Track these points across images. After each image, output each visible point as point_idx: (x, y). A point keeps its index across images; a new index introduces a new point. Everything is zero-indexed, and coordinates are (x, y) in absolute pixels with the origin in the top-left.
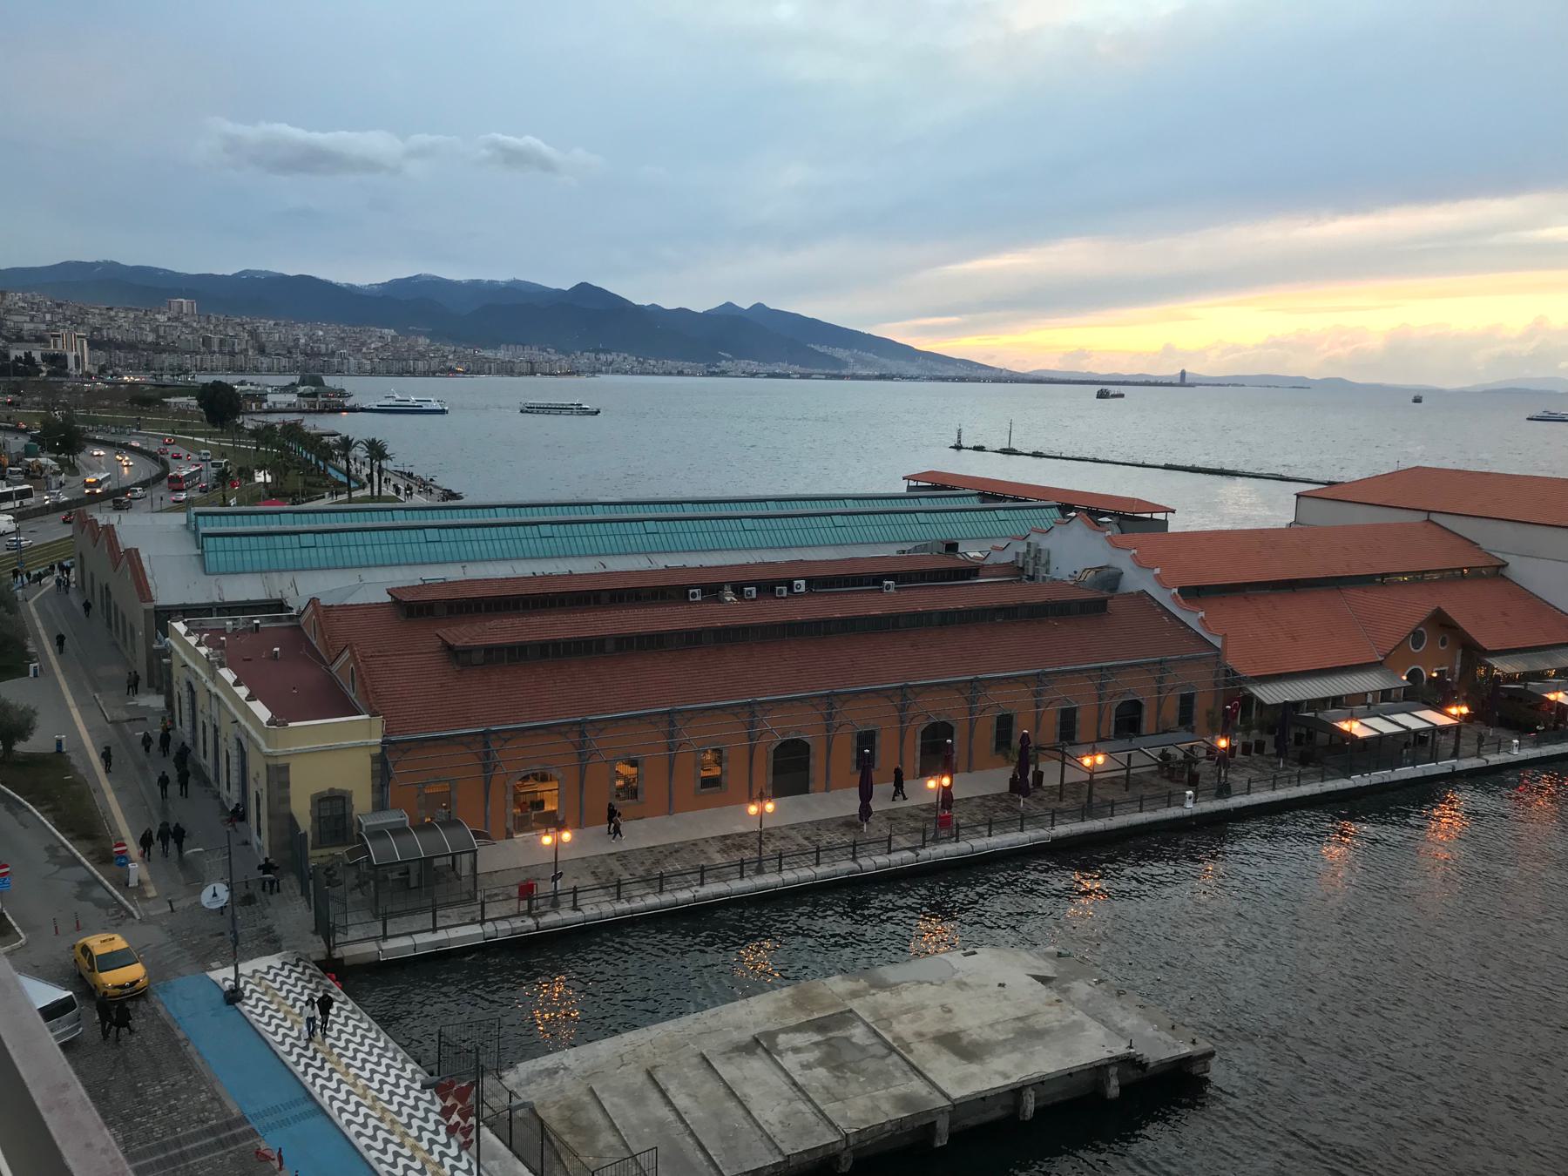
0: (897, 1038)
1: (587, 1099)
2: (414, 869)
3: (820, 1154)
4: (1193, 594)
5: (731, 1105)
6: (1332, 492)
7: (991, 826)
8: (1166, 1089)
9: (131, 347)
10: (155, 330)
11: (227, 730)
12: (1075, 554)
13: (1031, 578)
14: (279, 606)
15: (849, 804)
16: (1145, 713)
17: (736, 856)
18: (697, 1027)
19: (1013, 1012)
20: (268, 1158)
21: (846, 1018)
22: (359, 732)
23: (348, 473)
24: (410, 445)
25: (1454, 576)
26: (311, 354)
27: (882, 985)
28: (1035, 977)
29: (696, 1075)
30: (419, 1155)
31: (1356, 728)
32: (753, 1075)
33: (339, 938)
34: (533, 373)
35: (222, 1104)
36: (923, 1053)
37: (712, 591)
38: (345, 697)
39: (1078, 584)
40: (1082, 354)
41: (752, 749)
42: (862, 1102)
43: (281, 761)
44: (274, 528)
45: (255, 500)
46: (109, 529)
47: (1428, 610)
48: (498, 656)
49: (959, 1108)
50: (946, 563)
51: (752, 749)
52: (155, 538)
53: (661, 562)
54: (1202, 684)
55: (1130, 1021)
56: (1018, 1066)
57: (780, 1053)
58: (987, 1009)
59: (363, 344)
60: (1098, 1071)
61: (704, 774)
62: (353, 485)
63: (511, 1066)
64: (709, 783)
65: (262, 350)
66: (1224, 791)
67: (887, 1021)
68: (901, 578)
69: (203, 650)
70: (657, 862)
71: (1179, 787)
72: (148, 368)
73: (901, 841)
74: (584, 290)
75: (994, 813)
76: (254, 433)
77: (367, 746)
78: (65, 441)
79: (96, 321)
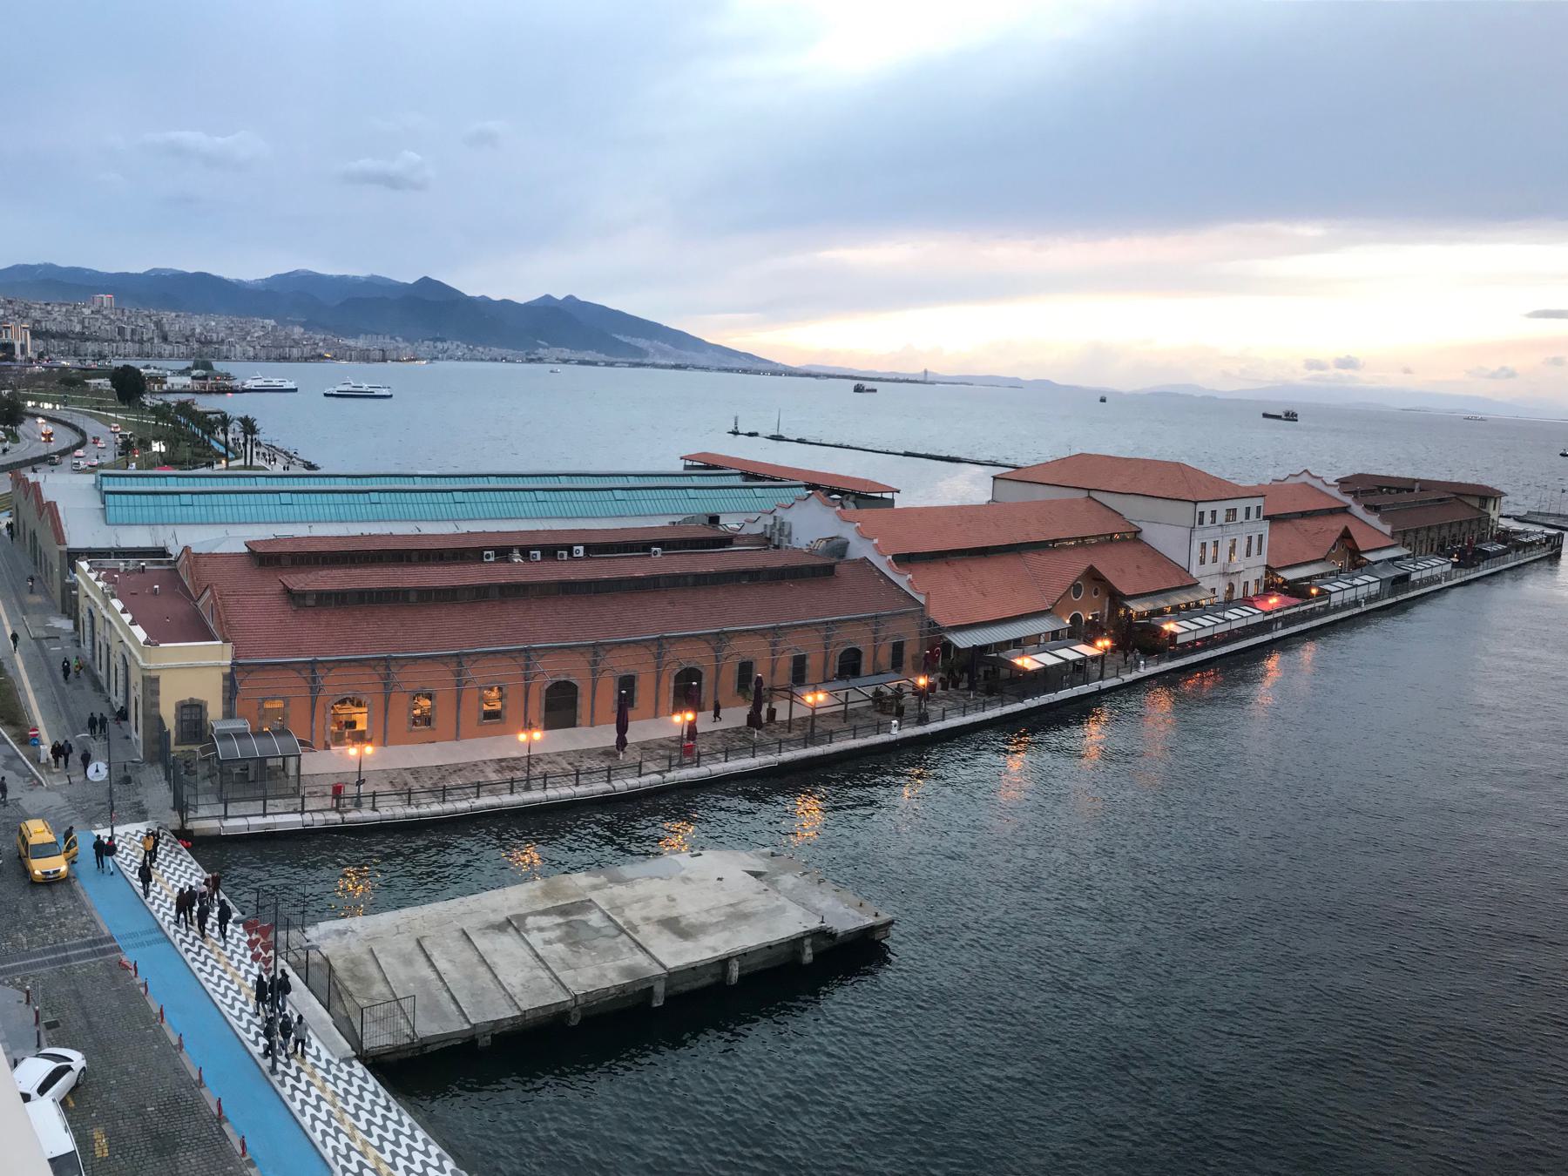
0: (628, 922)
1: (367, 957)
2: (252, 764)
3: (553, 1010)
4: (904, 560)
5: (482, 969)
6: (1012, 476)
7: (728, 753)
8: (850, 955)
9: (63, 336)
10: (82, 322)
11: (116, 649)
12: (812, 526)
13: (777, 547)
14: (162, 552)
15: (606, 736)
16: (864, 659)
17: (508, 775)
18: (462, 909)
19: (726, 900)
20: (127, 968)
22: (215, 655)
23: (226, 445)
25: (1108, 540)
26: (206, 342)
27: (619, 881)
28: (750, 873)
29: (457, 945)
30: (237, 980)
32: (507, 954)
33: (191, 814)
34: (384, 360)
35: (97, 926)
36: (647, 934)
37: (503, 553)
38: (206, 627)
39: (812, 552)
41: (527, 687)
43: (153, 674)
44: (159, 489)
45: (151, 466)
46: (36, 485)
49: (673, 976)
50: (709, 533)
51: (527, 687)
52: (68, 491)
53: (465, 527)
56: (727, 942)
57: (527, 931)
58: (706, 899)
59: (248, 333)
60: (795, 943)
61: (486, 707)
62: (230, 455)
63: (314, 923)
65: (165, 339)
66: (923, 719)
67: (620, 909)
68: (668, 545)
69: (100, 584)
70: (443, 778)
71: (887, 718)
72: (76, 354)
74: (426, 282)
75: (730, 744)
76: (155, 410)
77: (221, 666)
79: (36, 314)
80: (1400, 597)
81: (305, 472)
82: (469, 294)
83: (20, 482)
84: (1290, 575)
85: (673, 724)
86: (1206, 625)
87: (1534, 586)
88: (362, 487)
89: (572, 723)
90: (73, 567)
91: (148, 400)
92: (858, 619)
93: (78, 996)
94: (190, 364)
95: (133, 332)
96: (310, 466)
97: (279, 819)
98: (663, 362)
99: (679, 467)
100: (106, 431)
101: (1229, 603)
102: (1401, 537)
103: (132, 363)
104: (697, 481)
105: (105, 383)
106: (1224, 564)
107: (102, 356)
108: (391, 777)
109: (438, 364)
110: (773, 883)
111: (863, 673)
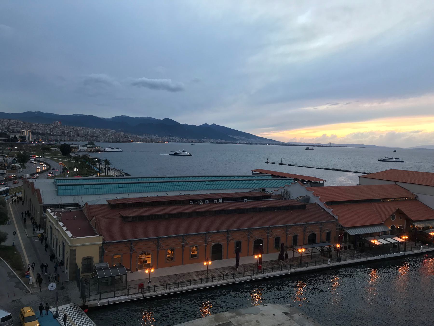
4: (330, 204)
6: (368, 176)
7: (273, 269)
9: (43, 134)
10: (50, 130)
11: (60, 239)
12: (297, 192)
14: (77, 205)
15: (232, 262)
22: (96, 240)
25: (404, 200)
27: (239, 314)
28: (284, 313)
33: (87, 299)
34: (152, 142)
37: (196, 201)
38: (93, 230)
41: (206, 246)
43: (74, 248)
44: (77, 183)
45: (73, 176)
46: (32, 183)
48: (141, 219)
50: (262, 194)
51: (206, 246)
53: (183, 193)
59: (106, 134)
61: (192, 253)
65: (78, 135)
66: (339, 260)
68: (249, 198)
69: (55, 217)
70: (178, 279)
71: (325, 259)
72: (47, 140)
73: (247, 273)
74: (167, 120)
75: (273, 266)
76: (75, 158)
79: (34, 127)
81: (125, 177)
82: (181, 123)
90: (45, 211)
91: (72, 155)
92: (315, 224)
94: (87, 143)
95: (68, 133)
96: (127, 175)
97: (120, 298)
98: (242, 142)
99: (250, 174)
100: (58, 165)
103: (67, 143)
104: (257, 178)
107: (57, 141)
108: (160, 279)
109: (171, 143)
110: (292, 317)
111: (317, 242)
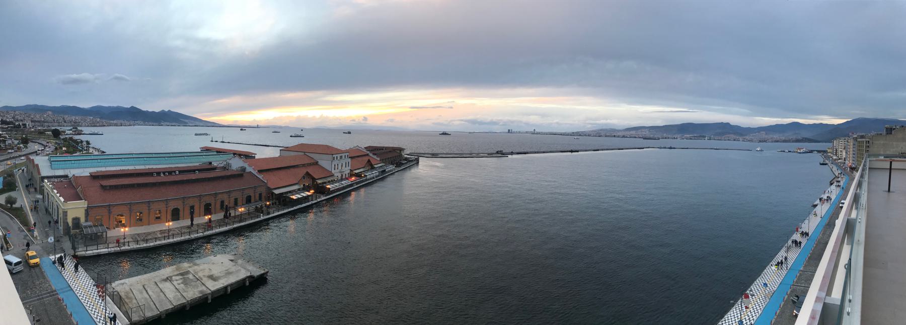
4: (260, 171)
6: (287, 149)
8: (257, 282)
9: (39, 122)
11: (55, 204)
12: (237, 164)
14: (66, 176)
15: (188, 222)
21: (188, 273)
22: (82, 204)
24: (95, 142)
25: (310, 165)
27: (195, 265)
31: (294, 197)
32: (167, 287)
36: (205, 280)
37: (158, 174)
40: (236, 121)
42: (191, 293)
47: (305, 172)
48: (116, 187)
49: (213, 293)
50: (210, 167)
53: (147, 167)
54: (263, 190)
55: (251, 268)
58: (218, 269)
60: (244, 280)
64: (157, 218)
66: (268, 214)
67: (196, 273)
68: (200, 170)
73: (200, 231)
75: (220, 223)
78: (25, 141)
80: (383, 176)
83: (28, 159)
84: (357, 171)
85: (119, 231)
86: (337, 185)
87: (414, 171)
88: (119, 157)
89: (178, 219)
93: (46, 311)
101: (342, 179)
102: (382, 161)
105: (50, 133)
106: (340, 169)
